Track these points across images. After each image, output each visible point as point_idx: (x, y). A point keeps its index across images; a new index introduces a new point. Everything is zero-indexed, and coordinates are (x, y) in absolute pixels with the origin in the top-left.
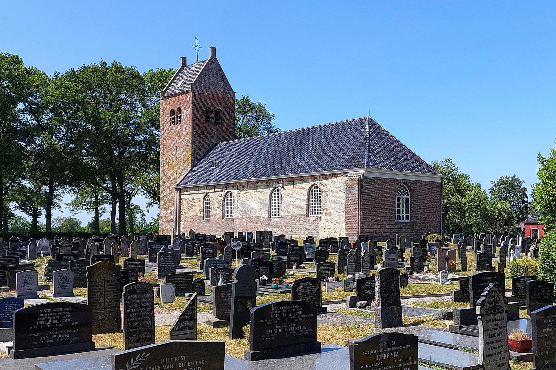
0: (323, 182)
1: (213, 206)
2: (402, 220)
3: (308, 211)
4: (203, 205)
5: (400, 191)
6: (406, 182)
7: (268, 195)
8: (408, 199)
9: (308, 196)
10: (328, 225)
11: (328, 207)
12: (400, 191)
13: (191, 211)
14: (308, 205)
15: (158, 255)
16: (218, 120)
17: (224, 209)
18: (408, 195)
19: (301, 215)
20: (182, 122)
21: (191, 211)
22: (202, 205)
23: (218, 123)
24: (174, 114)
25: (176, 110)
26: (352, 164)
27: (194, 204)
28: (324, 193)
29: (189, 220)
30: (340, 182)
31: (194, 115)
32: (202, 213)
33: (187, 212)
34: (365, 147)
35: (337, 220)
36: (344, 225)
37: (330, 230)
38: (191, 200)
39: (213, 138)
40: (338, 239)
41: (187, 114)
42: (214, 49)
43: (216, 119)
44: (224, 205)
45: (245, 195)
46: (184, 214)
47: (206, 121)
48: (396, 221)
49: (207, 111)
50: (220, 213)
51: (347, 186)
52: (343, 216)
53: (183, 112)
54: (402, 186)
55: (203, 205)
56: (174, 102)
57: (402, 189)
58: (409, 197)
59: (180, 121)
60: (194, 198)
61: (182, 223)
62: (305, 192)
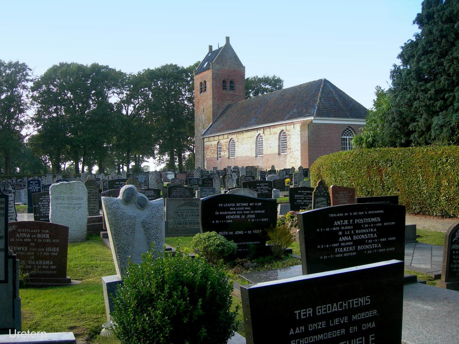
0: (288, 127)
1: (223, 150)
3: (279, 151)
5: (346, 133)
11: (292, 147)
12: (346, 133)
14: (279, 146)
16: (233, 87)
17: (229, 152)
19: (275, 154)
25: (203, 82)
26: (300, 115)
28: (288, 137)
29: (210, 160)
31: (214, 87)
39: (228, 100)
41: (209, 85)
42: (228, 39)
44: (229, 149)
47: (223, 89)
49: (224, 82)
51: (302, 130)
52: (299, 153)
53: (207, 83)
54: (348, 129)
56: (202, 77)
57: (348, 132)
59: (206, 90)
61: (205, 163)
62: (277, 136)
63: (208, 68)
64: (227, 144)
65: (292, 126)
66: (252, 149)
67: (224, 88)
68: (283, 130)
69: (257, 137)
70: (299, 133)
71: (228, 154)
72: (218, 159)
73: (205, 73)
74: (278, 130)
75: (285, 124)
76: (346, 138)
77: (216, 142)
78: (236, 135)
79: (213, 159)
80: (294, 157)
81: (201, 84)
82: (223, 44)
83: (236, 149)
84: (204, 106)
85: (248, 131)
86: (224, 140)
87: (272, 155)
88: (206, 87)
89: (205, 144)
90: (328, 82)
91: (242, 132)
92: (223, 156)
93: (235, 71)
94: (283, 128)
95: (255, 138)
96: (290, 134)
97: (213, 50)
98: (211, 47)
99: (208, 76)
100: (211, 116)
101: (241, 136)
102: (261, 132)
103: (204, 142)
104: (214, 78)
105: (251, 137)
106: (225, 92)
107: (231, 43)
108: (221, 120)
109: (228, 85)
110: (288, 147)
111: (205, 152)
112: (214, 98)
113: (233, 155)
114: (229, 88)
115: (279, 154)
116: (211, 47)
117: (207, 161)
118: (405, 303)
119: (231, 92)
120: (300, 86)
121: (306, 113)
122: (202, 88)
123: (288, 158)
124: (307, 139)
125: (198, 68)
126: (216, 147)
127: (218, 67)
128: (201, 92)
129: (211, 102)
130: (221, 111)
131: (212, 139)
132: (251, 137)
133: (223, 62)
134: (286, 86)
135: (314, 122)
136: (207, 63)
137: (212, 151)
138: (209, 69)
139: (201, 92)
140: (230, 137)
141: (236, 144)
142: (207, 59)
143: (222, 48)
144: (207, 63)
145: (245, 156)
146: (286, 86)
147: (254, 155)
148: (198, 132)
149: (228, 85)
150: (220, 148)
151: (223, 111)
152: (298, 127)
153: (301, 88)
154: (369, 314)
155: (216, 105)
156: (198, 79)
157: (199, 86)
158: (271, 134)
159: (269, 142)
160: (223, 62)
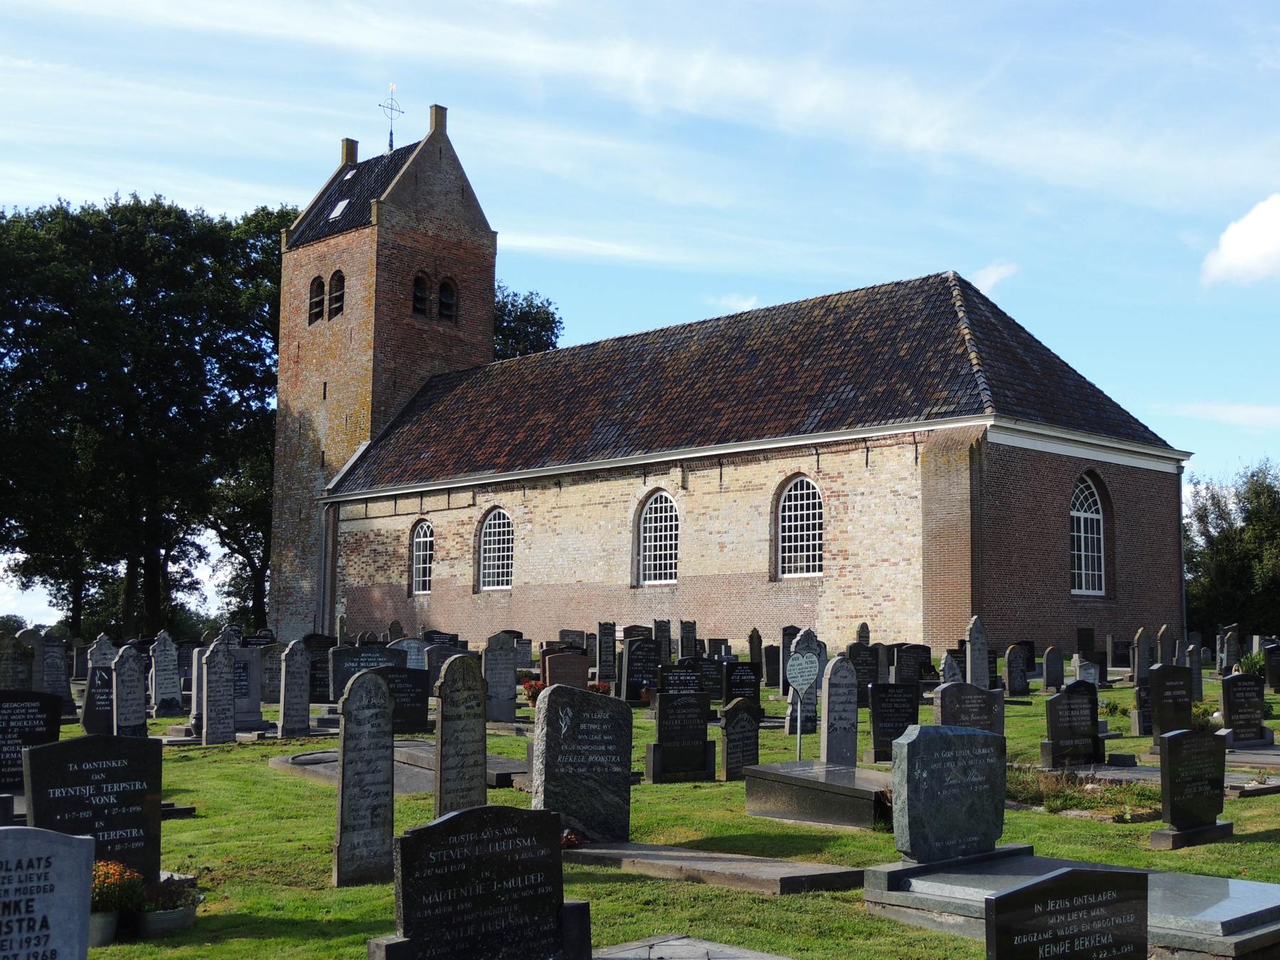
0: (830, 462)
2: (1084, 592)
4: (411, 551)
7: (631, 515)
8: (1098, 521)
9: (774, 512)
11: (851, 548)
13: (371, 569)
15: (445, 667)
16: (449, 307)
18: (1097, 512)
19: (750, 575)
23: (450, 318)
25: (327, 280)
27: (380, 548)
28: (833, 502)
32: (406, 576)
34: (909, 349)
35: (886, 589)
39: (433, 357)
42: (440, 114)
43: (443, 305)
44: (477, 551)
45: (548, 516)
47: (416, 310)
48: (1074, 592)
49: (419, 282)
50: (464, 572)
54: (1082, 481)
55: (411, 551)
58: (1100, 517)
59: (340, 309)
62: (765, 501)
64: (472, 528)
65: (857, 456)
67: (419, 306)
68: (799, 474)
69: (642, 504)
73: (341, 240)
74: (771, 473)
75: (816, 446)
76: (1079, 518)
77: (405, 524)
78: (518, 493)
80: (867, 591)
81: (317, 285)
82: (416, 130)
83: (516, 553)
84: (325, 378)
85: (592, 476)
87: (734, 583)
88: (340, 298)
91: (558, 481)
94: (805, 464)
96: (847, 489)
98: (351, 147)
99: (356, 255)
101: (545, 499)
103: (337, 520)
104: (384, 264)
105: (606, 505)
106: (419, 323)
107: (453, 131)
110: (834, 548)
112: (380, 344)
113: (504, 576)
114: (435, 310)
116: (351, 147)
121: (924, 403)
122: (321, 303)
123: (830, 593)
125: (314, 226)
127: (399, 218)
128: (314, 317)
129: (365, 359)
130: (402, 398)
132: (606, 505)
133: (413, 208)
134: (567, 339)
135: (993, 438)
137: (381, 561)
138: (367, 224)
139: (314, 317)
141: (519, 532)
143: (409, 149)
146: (567, 339)
148: (289, 478)
151: (413, 401)
153: (829, 311)
155: (385, 370)
156: (299, 269)
158: (722, 489)
159: (717, 526)
160: (413, 208)
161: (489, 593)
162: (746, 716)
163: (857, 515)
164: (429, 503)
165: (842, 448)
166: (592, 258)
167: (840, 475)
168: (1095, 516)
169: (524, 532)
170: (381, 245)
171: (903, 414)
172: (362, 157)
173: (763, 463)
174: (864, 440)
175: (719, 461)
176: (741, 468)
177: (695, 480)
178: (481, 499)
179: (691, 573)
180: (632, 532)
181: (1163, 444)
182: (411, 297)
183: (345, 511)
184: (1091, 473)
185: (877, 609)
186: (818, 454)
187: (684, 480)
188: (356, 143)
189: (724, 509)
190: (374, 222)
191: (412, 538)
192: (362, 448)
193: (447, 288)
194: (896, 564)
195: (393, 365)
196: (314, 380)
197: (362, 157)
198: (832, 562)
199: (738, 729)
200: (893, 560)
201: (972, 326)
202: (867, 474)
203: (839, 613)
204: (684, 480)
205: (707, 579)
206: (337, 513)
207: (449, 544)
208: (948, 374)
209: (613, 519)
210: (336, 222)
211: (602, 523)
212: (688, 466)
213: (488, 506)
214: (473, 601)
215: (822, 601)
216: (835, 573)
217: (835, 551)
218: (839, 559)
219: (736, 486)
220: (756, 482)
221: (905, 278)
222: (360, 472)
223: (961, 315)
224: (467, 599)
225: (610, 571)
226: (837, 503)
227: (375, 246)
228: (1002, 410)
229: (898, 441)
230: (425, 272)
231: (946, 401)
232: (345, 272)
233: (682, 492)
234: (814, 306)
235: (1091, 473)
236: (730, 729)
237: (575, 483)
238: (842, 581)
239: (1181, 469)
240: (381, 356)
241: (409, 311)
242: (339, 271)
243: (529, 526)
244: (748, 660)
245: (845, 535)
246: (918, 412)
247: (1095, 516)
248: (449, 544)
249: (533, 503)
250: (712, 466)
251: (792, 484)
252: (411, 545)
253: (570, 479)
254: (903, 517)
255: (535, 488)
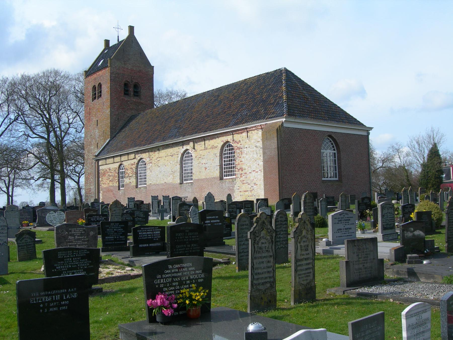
0: (237, 137)
4: (119, 175)
6: (330, 136)
7: (179, 159)
10: (244, 187)
11: (244, 167)
13: (108, 181)
18: (334, 150)
19: (214, 178)
20: (102, 96)
21: (108, 181)
22: (117, 175)
23: (137, 96)
24: (95, 91)
27: (110, 174)
28: (238, 151)
29: (109, 190)
30: (256, 136)
31: (113, 91)
32: (117, 183)
33: (105, 183)
34: (281, 98)
35: (254, 181)
36: (262, 187)
37: (247, 193)
38: (108, 170)
40: (255, 202)
41: (106, 89)
42: (131, 29)
43: (135, 92)
44: (137, 173)
45: (156, 161)
46: (103, 185)
47: (125, 94)
48: (323, 179)
49: (126, 85)
51: (265, 138)
52: (261, 176)
55: (119, 175)
56: (95, 79)
58: (336, 152)
59: (101, 96)
60: (109, 166)
61: (101, 195)
62: (218, 151)
63: (104, 67)
64: (134, 166)
65: (244, 134)
66: (173, 172)
67: (126, 93)
68: (228, 142)
69: (183, 155)
70: (260, 144)
71: (135, 181)
72: (119, 189)
73: (100, 73)
74: (219, 142)
77: (117, 165)
78: (147, 154)
79: (112, 188)
80: (249, 182)
81: (94, 88)
82: (124, 35)
83: (147, 174)
86: (129, 163)
87: (209, 180)
88: (101, 92)
89: (101, 168)
90: (290, 72)
92: (127, 184)
93: (140, 71)
94: (229, 138)
95: (180, 156)
96: (242, 146)
97: (110, 46)
98: (107, 42)
100: (109, 129)
102: (189, 147)
103: (98, 166)
104: (113, 80)
105: (172, 156)
106: (127, 98)
107: (136, 34)
108: (122, 135)
109: (131, 89)
111: (100, 179)
112: (112, 106)
114: (132, 94)
115: (221, 178)
117: (104, 192)
118: (60, 199)
119: (135, 99)
120: (245, 82)
121: (266, 114)
122: (95, 94)
123: (238, 183)
124: (274, 152)
126: (117, 171)
128: (94, 99)
129: (108, 111)
131: (111, 160)
132: (172, 156)
135: (285, 125)
136: (102, 61)
137: (111, 178)
139: (94, 99)
140: (138, 157)
141: (148, 166)
142: (102, 56)
143: (122, 41)
144: (102, 61)
145: (163, 182)
147: (177, 180)
149: (131, 89)
150: (122, 173)
151: (125, 124)
152: (256, 136)
154: (58, 198)
157: (91, 91)
158: (206, 149)
159: (204, 161)
161: (140, 188)
162: (27, 236)
163: (245, 155)
164: (123, 158)
165: (240, 132)
166: (182, 73)
167: (240, 141)
168: (334, 152)
169: (150, 166)
170: (111, 73)
171: (260, 119)
172: (111, 45)
173: (217, 139)
174: (246, 128)
175: (204, 139)
176: (210, 141)
177: (197, 146)
178: (137, 156)
179: (197, 178)
180: (180, 165)
181: (363, 125)
182: (123, 90)
183: (100, 163)
184: (330, 136)
185: (252, 188)
186: (233, 135)
187: (194, 146)
188: (109, 41)
189: (205, 156)
190: (109, 65)
191: (119, 170)
192: (108, 141)
193: (136, 86)
194: (257, 172)
195: (117, 113)
196: (94, 119)
197: (111, 45)
198: (238, 172)
199: (23, 241)
200: (256, 171)
201: (287, 86)
202: (248, 141)
203: (241, 190)
204: (194, 146)
205: (202, 180)
206: (98, 163)
207: (129, 172)
208: (275, 103)
209: (174, 161)
210: (100, 67)
211: (171, 162)
212: (195, 141)
213: (139, 158)
214: (136, 191)
215: (236, 186)
216: (239, 176)
217: (239, 168)
218: (240, 171)
219: (209, 147)
220: (215, 145)
221: (270, 71)
222: (106, 149)
223: (283, 82)
224: (134, 190)
225: (174, 179)
226: (239, 151)
227: (109, 74)
228: (291, 114)
229: (256, 128)
230: (127, 81)
231: (273, 113)
232: (102, 83)
233: (194, 150)
234: (242, 83)
235: (330, 136)
236: (19, 242)
237: (163, 149)
238: (242, 179)
239: (369, 134)
240: (113, 110)
241: (123, 95)
242: (100, 83)
243: (151, 164)
244: (372, 204)
245: (242, 163)
246: (264, 118)
247: (334, 152)
248: (129, 172)
249: (152, 157)
250: (202, 141)
251: (226, 146)
252: (119, 173)
253: (161, 148)
254: (259, 155)
255: (152, 151)
